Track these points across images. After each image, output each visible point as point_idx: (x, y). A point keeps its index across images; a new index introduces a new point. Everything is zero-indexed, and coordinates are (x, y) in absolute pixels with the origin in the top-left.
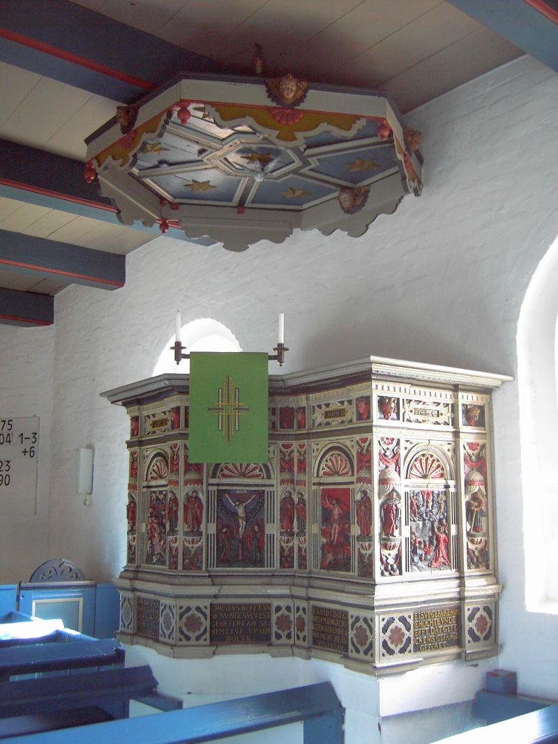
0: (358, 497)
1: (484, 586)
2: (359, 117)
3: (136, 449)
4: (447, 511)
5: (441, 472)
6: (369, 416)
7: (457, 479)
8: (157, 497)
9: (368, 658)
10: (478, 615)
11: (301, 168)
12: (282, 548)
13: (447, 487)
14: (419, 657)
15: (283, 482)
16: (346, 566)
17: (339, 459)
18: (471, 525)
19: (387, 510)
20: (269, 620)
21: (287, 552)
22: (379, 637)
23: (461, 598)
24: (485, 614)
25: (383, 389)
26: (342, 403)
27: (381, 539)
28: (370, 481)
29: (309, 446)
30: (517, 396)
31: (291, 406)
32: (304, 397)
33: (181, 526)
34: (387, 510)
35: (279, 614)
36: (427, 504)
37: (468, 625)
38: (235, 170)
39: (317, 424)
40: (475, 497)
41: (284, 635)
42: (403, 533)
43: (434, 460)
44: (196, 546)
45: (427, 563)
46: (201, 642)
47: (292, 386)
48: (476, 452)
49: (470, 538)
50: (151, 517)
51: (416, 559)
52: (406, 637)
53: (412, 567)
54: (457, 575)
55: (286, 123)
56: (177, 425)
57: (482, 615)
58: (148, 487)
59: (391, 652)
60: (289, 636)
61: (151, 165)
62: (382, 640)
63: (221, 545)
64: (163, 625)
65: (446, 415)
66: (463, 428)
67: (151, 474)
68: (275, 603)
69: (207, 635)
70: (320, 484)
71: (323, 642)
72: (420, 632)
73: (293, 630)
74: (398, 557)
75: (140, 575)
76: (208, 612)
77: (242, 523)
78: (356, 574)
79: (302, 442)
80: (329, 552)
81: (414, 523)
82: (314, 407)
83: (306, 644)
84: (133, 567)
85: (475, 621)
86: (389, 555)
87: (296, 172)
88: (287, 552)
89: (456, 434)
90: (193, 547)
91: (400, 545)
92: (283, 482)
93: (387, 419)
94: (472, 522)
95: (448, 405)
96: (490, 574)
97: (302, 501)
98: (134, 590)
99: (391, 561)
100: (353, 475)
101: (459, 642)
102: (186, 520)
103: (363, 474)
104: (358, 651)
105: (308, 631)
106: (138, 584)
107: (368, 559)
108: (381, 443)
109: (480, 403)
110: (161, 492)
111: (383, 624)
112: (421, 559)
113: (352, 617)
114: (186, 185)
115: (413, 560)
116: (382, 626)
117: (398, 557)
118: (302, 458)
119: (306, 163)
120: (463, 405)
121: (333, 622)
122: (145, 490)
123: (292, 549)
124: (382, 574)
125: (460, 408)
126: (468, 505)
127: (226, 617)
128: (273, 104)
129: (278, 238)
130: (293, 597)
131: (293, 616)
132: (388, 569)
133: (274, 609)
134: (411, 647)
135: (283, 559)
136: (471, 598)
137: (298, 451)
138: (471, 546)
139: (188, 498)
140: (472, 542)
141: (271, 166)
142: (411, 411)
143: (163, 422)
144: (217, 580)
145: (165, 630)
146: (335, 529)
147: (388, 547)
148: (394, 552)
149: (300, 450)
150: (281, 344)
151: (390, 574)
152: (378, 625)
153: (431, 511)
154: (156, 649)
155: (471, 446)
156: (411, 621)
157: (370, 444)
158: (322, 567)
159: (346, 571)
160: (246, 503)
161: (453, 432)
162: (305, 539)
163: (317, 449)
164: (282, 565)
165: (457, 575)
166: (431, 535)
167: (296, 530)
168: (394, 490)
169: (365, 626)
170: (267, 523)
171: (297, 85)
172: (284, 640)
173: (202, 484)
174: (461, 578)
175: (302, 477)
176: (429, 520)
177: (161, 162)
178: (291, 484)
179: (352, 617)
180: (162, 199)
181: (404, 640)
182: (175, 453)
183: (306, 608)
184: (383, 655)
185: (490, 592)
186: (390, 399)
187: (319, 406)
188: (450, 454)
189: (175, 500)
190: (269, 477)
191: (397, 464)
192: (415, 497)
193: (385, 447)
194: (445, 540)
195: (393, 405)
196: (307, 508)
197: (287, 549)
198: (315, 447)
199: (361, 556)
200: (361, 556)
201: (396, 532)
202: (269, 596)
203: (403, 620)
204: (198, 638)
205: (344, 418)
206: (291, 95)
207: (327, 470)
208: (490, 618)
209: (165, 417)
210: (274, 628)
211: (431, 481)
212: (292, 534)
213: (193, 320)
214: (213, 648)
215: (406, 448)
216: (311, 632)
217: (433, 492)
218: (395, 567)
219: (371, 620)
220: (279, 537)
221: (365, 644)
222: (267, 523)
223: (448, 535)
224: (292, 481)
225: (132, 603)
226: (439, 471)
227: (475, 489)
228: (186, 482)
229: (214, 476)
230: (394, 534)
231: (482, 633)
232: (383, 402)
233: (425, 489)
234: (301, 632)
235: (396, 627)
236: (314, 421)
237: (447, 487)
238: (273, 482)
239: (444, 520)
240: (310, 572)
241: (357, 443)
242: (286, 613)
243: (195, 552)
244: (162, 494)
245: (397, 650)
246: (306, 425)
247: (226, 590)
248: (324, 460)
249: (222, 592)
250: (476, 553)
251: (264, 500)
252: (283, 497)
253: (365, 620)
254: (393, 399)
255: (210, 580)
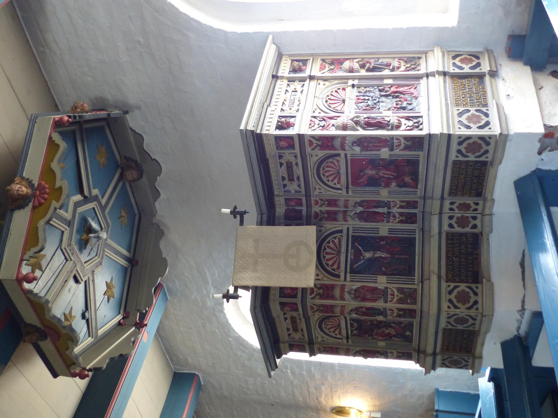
0: (357, 149)
1: (434, 59)
2: (50, 138)
3: (316, 347)
4: (373, 86)
5: (341, 90)
6: (290, 138)
7: (348, 78)
8: (356, 329)
9: (492, 142)
10: (459, 64)
11: (100, 204)
12: (401, 222)
13: (353, 86)
14: (493, 104)
15: (345, 220)
16: (414, 164)
17: (327, 169)
18: (385, 69)
19: (368, 125)
20: (461, 234)
21: (403, 218)
22: (474, 131)
23: (445, 74)
24: (458, 59)
25: (270, 126)
26: (281, 164)
27: (392, 129)
28: (344, 138)
29: (316, 196)
30: (285, 33)
31: (284, 211)
32: (276, 199)
33: (380, 304)
34: (368, 125)
35: (455, 225)
36: (366, 100)
37: (467, 69)
38: (97, 258)
39: (298, 189)
40: (362, 66)
41: (473, 222)
42: (391, 117)
43: (331, 95)
44: (396, 293)
45: (414, 100)
46: (479, 291)
47: (267, 209)
48: (327, 66)
49: (396, 69)
50: (372, 335)
51: (410, 107)
52: (475, 113)
53: (417, 110)
54: (425, 79)
55: (48, 194)
56: (295, 306)
57: (459, 61)
58: (347, 338)
59: (487, 124)
60: (475, 218)
61: (86, 326)
62: (477, 130)
63: (396, 272)
64: (465, 325)
65: (297, 85)
66: (306, 74)
67: (336, 334)
68: (446, 228)
69: (473, 286)
70: (347, 188)
71: (479, 187)
72: (471, 104)
73: (469, 214)
74: (408, 118)
75: (422, 348)
76: (452, 285)
77: (378, 254)
78: (420, 153)
79: (313, 202)
80: (403, 179)
81: (380, 109)
82: (285, 191)
83: (481, 203)
84: (415, 355)
85: (464, 66)
86: (405, 124)
87: (103, 208)
88: (403, 218)
89: (311, 78)
90: (397, 296)
91: (398, 117)
92: (345, 220)
93: (294, 124)
94: (383, 68)
95: (288, 85)
96: (426, 56)
97: (360, 204)
98: (434, 354)
99: (410, 123)
100: (339, 155)
101: (481, 77)
102: (375, 300)
103: (337, 144)
104: (487, 152)
105: (470, 201)
106: (430, 349)
107: (408, 142)
108: (313, 128)
109: (289, 62)
110: (352, 325)
111: (463, 129)
112: (410, 104)
113: (457, 157)
114: (108, 301)
115: (411, 110)
116: (465, 129)
117: (408, 118)
118: (326, 203)
119: (96, 198)
120: (289, 74)
121: (462, 177)
122: (350, 341)
123: (401, 214)
124: (421, 130)
125: (292, 75)
126: (369, 70)
127: (457, 269)
128: (31, 205)
129: (160, 233)
130: (441, 213)
131: (458, 214)
132: (418, 126)
133: (452, 229)
134: (484, 109)
135: (409, 221)
136: (444, 67)
137: (321, 206)
138: (403, 68)
139: (356, 298)
140: (398, 68)
141: (95, 225)
142: (290, 109)
143: (294, 321)
144: (426, 276)
145: (469, 324)
146: (384, 174)
147: (398, 124)
148: (403, 121)
149: (320, 204)
150: (231, 211)
151: (421, 124)
152: (465, 132)
153: (372, 97)
154: (486, 333)
155: (322, 68)
156: (462, 109)
157: (313, 137)
158: (416, 187)
159: (419, 163)
160: (362, 250)
161: (310, 81)
162: (393, 202)
163: (320, 189)
164: (414, 222)
165: (425, 79)
166: (391, 97)
167: (385, 210)
168: (352, 120)
169: (465, 144)
170: (378, 233)
171: (16, 184)
172: (478, 222)
173: (345, 285)
174: (427, 75)
175: (341, 203)
176: (379, 98)
177: (83, 316)
178: (347, 212)
179: (457, 157)
180: (119, 324)
181: (477, 114)
182: (318, 308)
183: (450, 201)
184: (490, 128)
185: (440, 54)
186: (278, 121)
187: (285, 186)
188: (327, 83)
189: (357, 310)
190: (341, 231)
191: (331, 118)
192: (360, 108)
193: (316, 126)
194: (397, 88)
195: (283, 120)
196: (367, 199)
197: (401, 218)
198: (318, 191)
199: (407, 148)
200: (407, 148)
201: (388, 119)
202: (440, 233)
203: (460, 114)
204: (476, 294)
205: (294, 163)
206: (24, 189)
207: (336, 181)
208: (461, 55)
209: (289, 319)
210: (468, 230)
211: (348, 96)
212: (389, 213)
213: (225, 314)
214: (484, 280)
215: (320, 113)
216: (471, 198)
217: (357, 96)
218: (415, 121)
219: (460, 138)
220: (390, 224)
221: (480, 144)
222: (378, 233)
223: (392, 86)
224: (345, 212)
225: (446, 357)
226: (340, 91)
227: (356, 66)
228: (343, 299)
229: (338, 276)
230: (389, 120)
231: (474, 61)
232: (280, 127)
233: (354, 101)
234: (471, 207)
235: (466, 119)
236: (296, 192)
237: (353, 86)
238: (345, 228)
239: (380, 88)
240: (420, 198)
241: (313, 149)
242: (455, 219)
243: (401, 294)
244: (353, 324)
245: (486, 119)
246: (299, 198)
247: (434, 266)
248: (327, 182)
249: (436, 271)
250: (408, 65)
251: (360, 236)
252: (357, 219)
253: (460, 143)
254: (279, 120)
255: (426, 281)
